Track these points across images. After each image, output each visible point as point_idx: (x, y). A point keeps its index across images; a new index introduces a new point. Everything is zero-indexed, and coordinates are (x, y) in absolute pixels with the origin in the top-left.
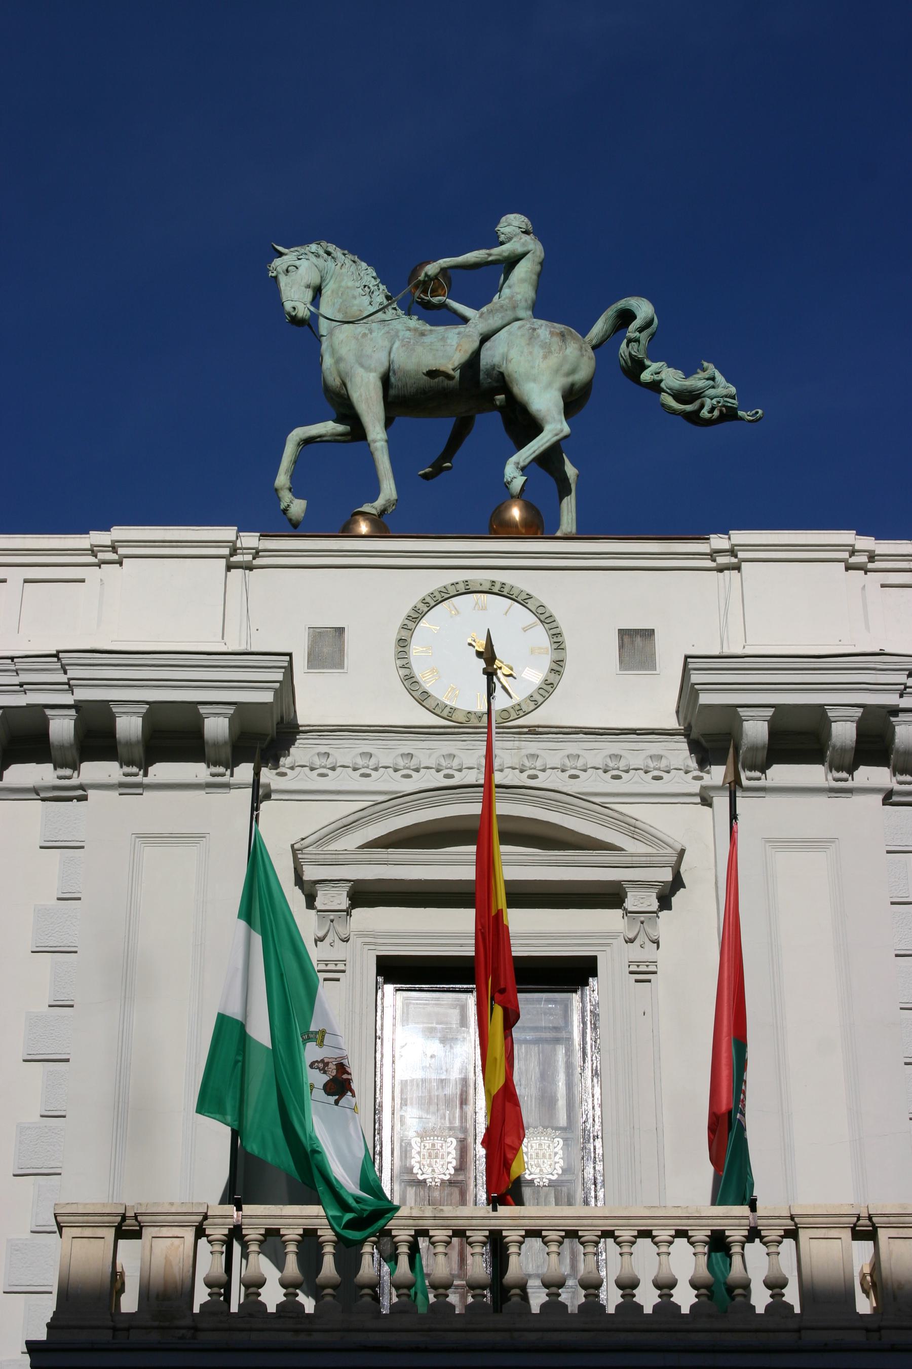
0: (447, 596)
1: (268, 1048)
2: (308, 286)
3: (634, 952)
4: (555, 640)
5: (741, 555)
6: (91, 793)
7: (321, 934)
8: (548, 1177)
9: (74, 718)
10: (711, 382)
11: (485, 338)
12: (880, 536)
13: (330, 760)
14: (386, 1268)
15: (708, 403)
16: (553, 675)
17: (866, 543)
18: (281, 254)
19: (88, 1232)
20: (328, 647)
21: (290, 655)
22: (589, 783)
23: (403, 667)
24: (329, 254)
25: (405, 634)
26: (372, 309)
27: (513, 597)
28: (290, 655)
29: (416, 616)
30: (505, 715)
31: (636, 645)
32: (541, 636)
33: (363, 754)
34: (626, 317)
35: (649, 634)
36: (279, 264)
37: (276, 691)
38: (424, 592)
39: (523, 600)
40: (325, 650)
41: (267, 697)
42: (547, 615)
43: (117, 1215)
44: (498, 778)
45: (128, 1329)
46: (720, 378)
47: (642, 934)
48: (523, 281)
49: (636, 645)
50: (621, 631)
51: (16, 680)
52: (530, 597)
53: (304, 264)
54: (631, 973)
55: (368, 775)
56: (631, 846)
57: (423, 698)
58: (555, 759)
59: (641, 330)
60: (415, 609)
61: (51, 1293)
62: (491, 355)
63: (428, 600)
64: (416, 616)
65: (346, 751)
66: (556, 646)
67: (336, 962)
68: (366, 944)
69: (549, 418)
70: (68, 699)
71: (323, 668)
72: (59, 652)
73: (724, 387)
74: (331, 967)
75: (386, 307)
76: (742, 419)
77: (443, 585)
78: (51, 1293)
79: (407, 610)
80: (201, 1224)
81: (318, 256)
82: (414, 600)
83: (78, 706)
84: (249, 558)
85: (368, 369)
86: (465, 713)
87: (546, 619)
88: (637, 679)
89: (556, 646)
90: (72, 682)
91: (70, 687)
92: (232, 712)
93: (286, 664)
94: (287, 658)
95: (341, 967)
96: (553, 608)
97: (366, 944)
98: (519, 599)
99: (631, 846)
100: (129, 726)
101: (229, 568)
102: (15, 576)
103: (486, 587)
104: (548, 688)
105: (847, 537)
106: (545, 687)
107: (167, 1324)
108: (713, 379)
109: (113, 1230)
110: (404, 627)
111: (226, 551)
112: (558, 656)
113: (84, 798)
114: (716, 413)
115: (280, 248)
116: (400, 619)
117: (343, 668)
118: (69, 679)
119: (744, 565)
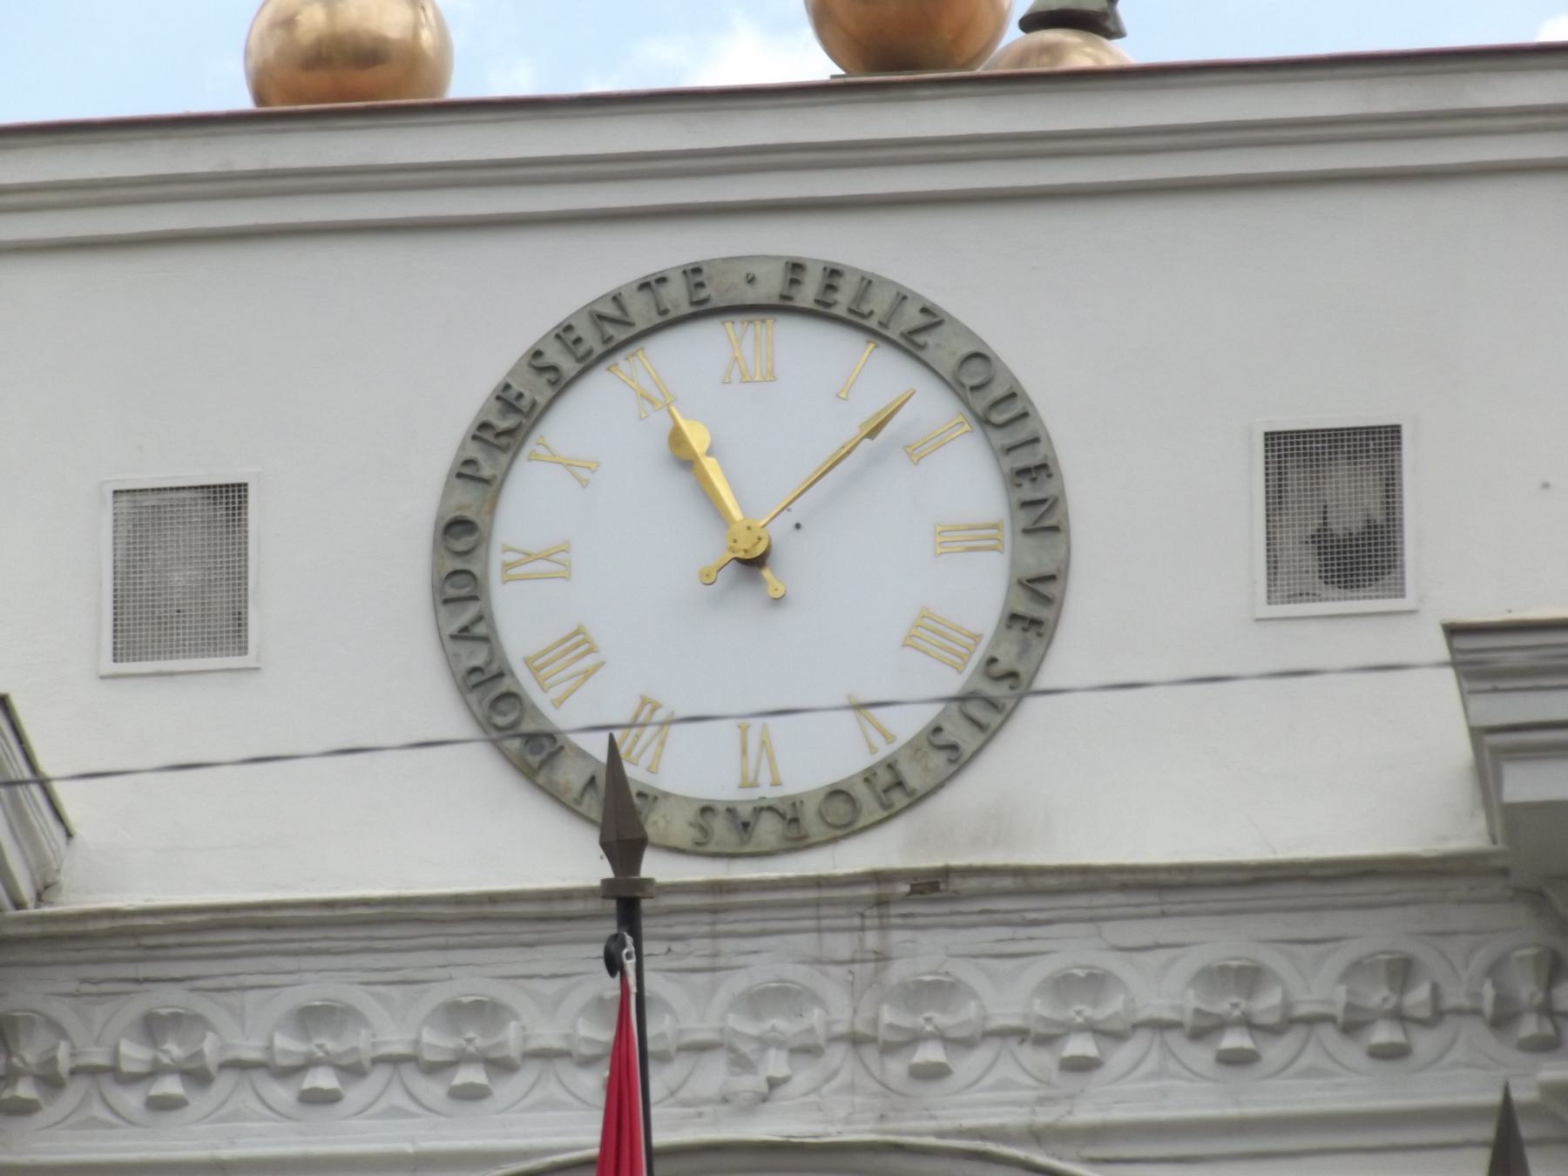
0: (620, 334)
1: (597, 762)
4: (1028, 492)
14: (905, 888)
16: (1016, 633)
20: (183, 570)
25: (467, 500)
27: (872, 323)
29: (506, 426)
31: (1335, 510)
35: (1378, 446)
39: (912, 331)
40: (177, 578)
42: (997, 391)
49: (1335, 510)
50: (1273, 440)
52: (933, 318)
55: (327, 1098)
58: (1009, 995)
64: (506, 426)
66: (1026, 518)
71: (172, 653)
79: (470, 399)
82: (494, 361)
86: (691, 813)
87: (996, 405)
88: (1341, 629)
89: (1026, 518)
96: (1027, 362)
98: (893, 333)
104: (999, 691)
110: (465, 472)
116: (446, 439)
117: (243, 649)
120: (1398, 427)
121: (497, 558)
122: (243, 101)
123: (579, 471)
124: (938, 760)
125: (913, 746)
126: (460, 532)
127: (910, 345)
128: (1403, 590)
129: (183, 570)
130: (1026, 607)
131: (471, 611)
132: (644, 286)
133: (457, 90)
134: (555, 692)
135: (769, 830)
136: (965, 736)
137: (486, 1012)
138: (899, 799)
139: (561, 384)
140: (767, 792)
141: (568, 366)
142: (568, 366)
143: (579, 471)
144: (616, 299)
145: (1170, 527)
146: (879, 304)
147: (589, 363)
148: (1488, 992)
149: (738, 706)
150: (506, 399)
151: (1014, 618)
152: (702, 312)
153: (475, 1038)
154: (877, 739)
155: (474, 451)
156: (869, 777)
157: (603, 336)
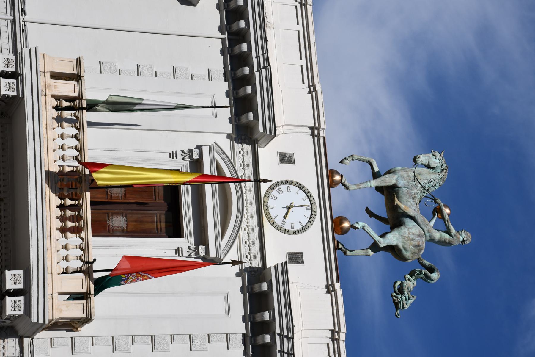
2: (429, 162)
5: (333, 293)
7: (185, 151)
10: (407, 298)
11: (413, 219)
12: (347, 342)
13: (251, 232)
15: (399, 296)
17: (343, 337)
18: (440, 154)
19: (85, 308)
20: (286, 159)
22: (243, 234)
23: (282, 182)
24: (443, 170)
25: (294, 183)
26: (422, 184)
29: (301, 187)
30: (268, 214)
31: (296, 258)
32: (298, 227)
33: (247, 152)
34: (432, 270)
36: (437, 154)
38: (310, 189)
44: (243, 184)
46: (410, 302)
47: (191, 251)
48: (441, 235)
49: (296, 258)
53: (437, 161)
54: (173, 152)
56: (223, 243)
59: (425, 275)
60: (303, 187)
62: (409, 223)
64: (301, 187)
65: (249, 159)
67: (176, 156)
68: (183, 166)
69: (385, 239)
73: (408, 304)
74: (174, 155)
75: (424, 189)
76: (397, 311)
79: (303, 184)
81: (442, 166)
82: (307, 186)
85: (397, 180)
87: (304, 229)
91: (259, 70)
95: (175, 158)
96: (308, 232)
97: (183, 166)
99: (223, 243)
103: (314, 209)
104: (279, 228)
105: (343, 329)
108: (409, 299)
110: (297, 183)
111: (285, 334)
112: (291, 232)
114: (395, 298)
115: (443, 153)
116: (299, 182)
119: (329, 294)
120: (51, 79)
122: (329, 169)
126: (295, 233)
127: (309, 222)
128: (299, 253)
129: (286, 159)
130: (286, 231)
133: (331, 189)
135: (266, 208)
140: (269, 208)
145: (295, 244)
146: (313, 219)
157: (309, 196)
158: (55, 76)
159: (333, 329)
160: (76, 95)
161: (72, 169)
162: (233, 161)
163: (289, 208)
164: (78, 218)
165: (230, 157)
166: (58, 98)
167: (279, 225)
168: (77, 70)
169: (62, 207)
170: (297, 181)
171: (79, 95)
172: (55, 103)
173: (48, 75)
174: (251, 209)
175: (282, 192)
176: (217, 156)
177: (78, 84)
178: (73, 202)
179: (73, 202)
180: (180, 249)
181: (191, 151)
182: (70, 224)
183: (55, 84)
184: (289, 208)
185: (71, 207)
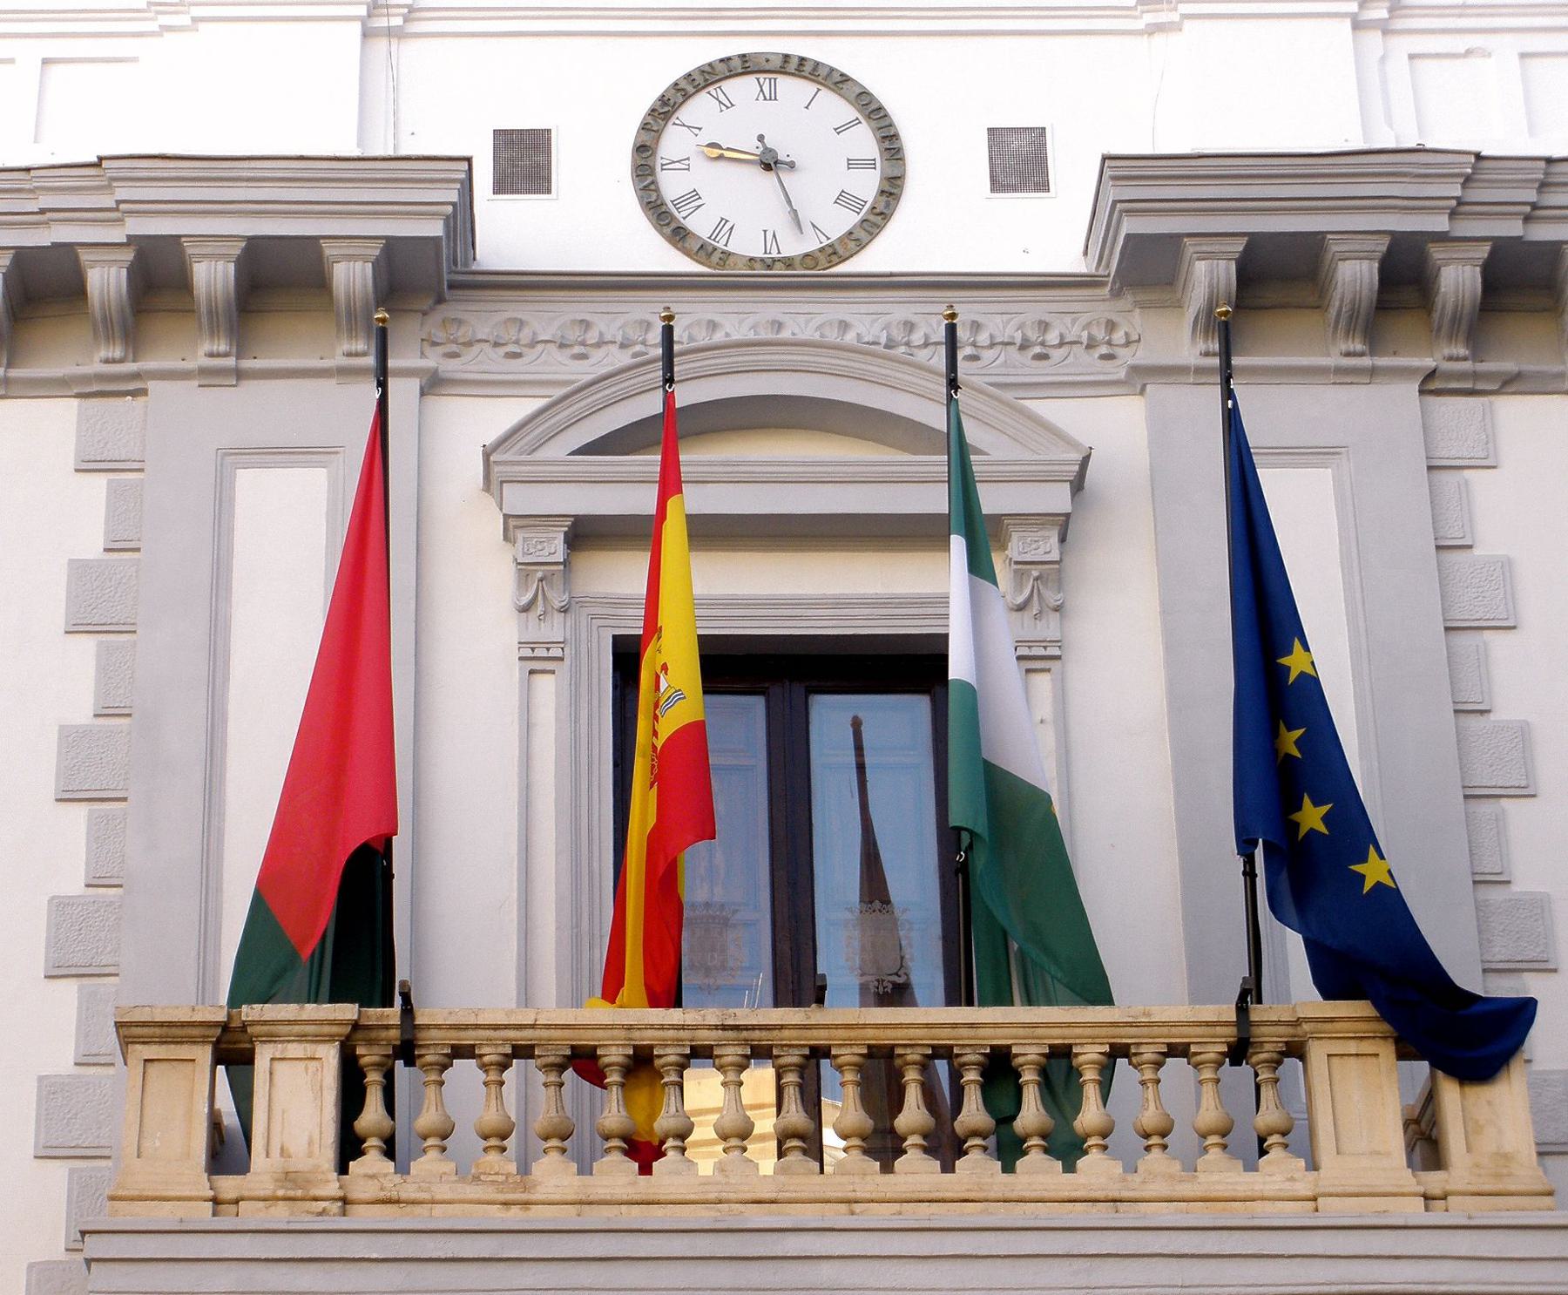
3: (1029, 628)
6: (152, 385)
7: (1020, 600)
8: (895, 979)
9: (127, 264)
16: (884, 198)
20: (525, 161)
21: (469, 160)
28: (469, 160)
31: (1019, 162)
37: (447, 220)
41: (435, 229)
42: (873, 107)
43: (216, 1024)
45: (236, 1202)
51: (33, 206)
54: (1019, 658)
57: (679, 236)
61: (857, 724)
63: (683, 85)
70: (117, 235)
72: (101, 159)
77: (708, 61)
78: (857, 724)
80: (348, 1037)
83: (132, 240)
84: (397, 21)
90: (122, 206)
92: (377, 252)
93: (463, 176)
94: (465, 166)
100: (213, 276)
101: (367, 34)
102: (29, 53)
106: (872, 218)
107: (299, 1193)
109: (208, 1049)
110: (645, 127)
113: (143, 392)
118: (118, 202)
121: (659, 162)
123: (843, 198)
124: (852, 245)
125: (840, 239)
131: (650, 179)
132: (722, 60)
134: (684, 214)
136: (862, 235)
137: (586, 325)
138: (835, 259)
139: (687, 97)
141: (691, 89)
142: (691, 89)
143: (843, 198)
144: (710, 64)
147: (698, 89)
148: (1085, 334)
149: (744, 217)
150: (663, 100)
151: (883, 192)
152: (746, 72)
153: (513, 333)
154: (823, 239)
155: (649, 120)
156: (822, 250)
158: (226, 1151)
159: (1348, 23)
160: (330, 1055)
161: (791, 1094)
162: (559, 392)
163: (769, 163)
164: (999, 1068)
165: (540, 403)
166: (349, 1147)
167: (857, 218)
168: (192, 1041)
169: (1009, 1150)
170: (672, 81)
171: (329, 1038)
172: (372, 1162)
173: (229, 1185)
174: (806, 318)
175: (695, 195)
176: (558, 450)
177: (271, 1038)
178: (913, 1095)
179: (913, 1095)
180: (1024, 651)
181: (525, 570)
182: (973, 1113)
183: (275, 1151)
184: (769, 163)
185: (943, 1107)
